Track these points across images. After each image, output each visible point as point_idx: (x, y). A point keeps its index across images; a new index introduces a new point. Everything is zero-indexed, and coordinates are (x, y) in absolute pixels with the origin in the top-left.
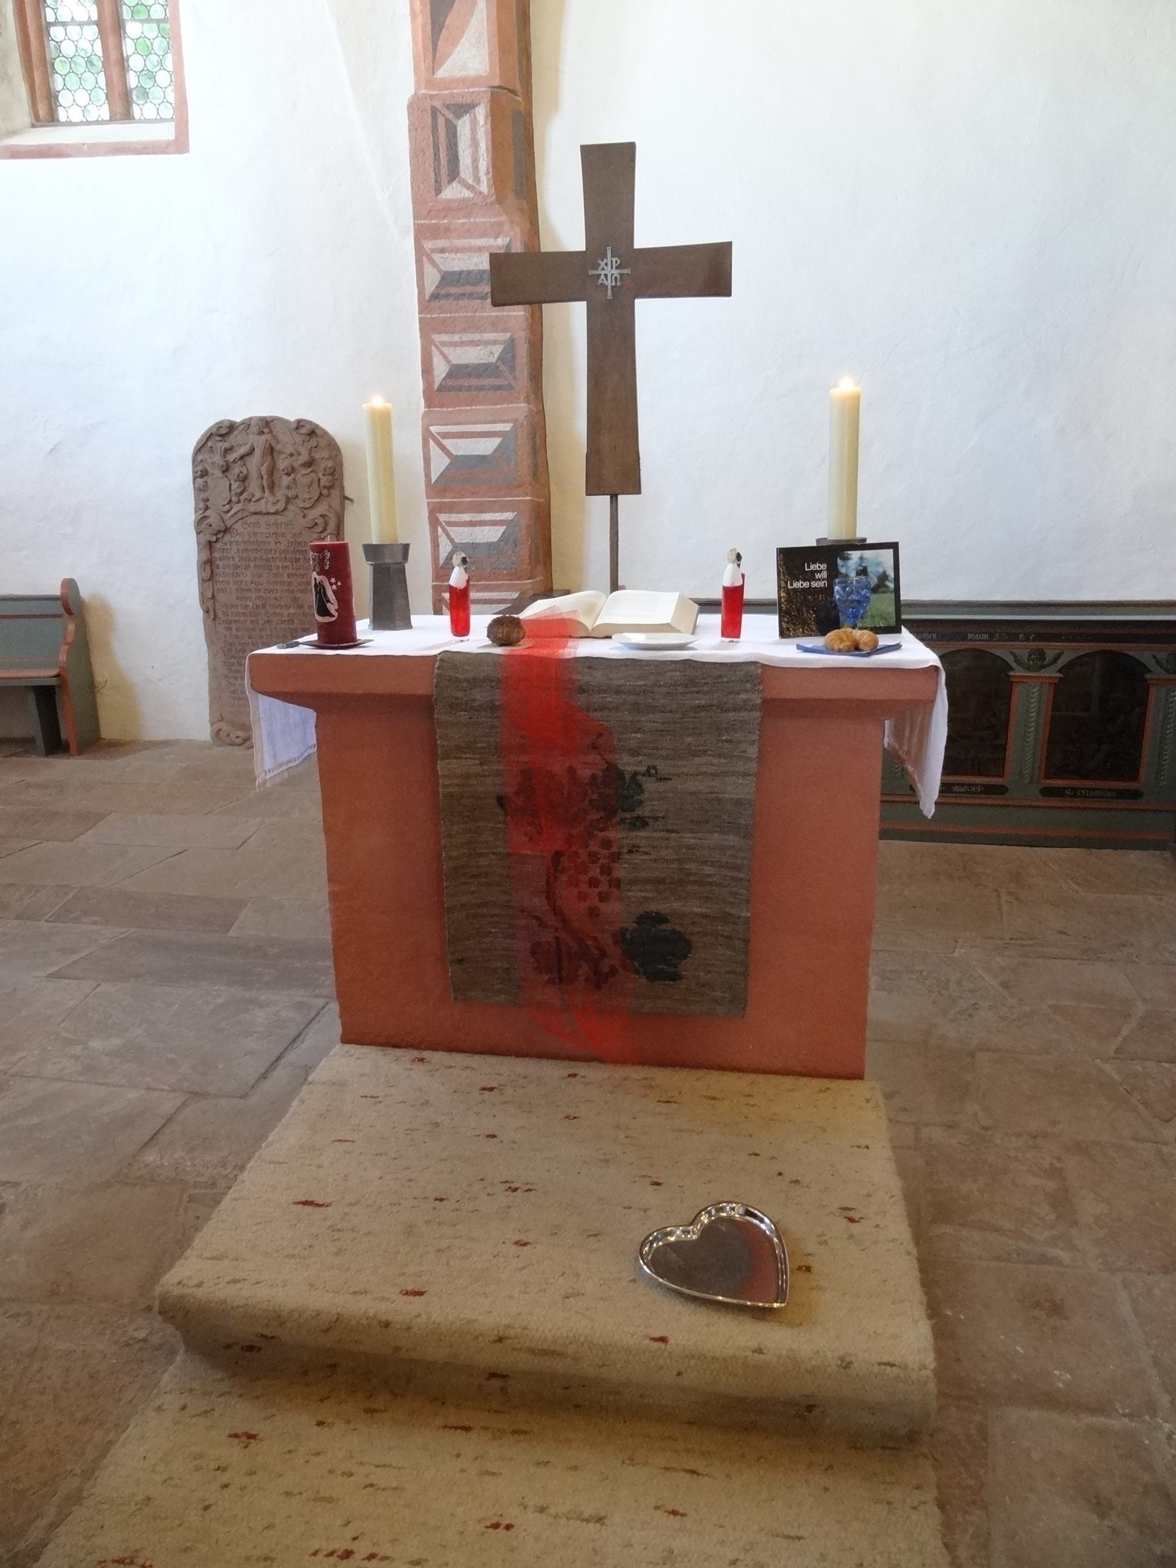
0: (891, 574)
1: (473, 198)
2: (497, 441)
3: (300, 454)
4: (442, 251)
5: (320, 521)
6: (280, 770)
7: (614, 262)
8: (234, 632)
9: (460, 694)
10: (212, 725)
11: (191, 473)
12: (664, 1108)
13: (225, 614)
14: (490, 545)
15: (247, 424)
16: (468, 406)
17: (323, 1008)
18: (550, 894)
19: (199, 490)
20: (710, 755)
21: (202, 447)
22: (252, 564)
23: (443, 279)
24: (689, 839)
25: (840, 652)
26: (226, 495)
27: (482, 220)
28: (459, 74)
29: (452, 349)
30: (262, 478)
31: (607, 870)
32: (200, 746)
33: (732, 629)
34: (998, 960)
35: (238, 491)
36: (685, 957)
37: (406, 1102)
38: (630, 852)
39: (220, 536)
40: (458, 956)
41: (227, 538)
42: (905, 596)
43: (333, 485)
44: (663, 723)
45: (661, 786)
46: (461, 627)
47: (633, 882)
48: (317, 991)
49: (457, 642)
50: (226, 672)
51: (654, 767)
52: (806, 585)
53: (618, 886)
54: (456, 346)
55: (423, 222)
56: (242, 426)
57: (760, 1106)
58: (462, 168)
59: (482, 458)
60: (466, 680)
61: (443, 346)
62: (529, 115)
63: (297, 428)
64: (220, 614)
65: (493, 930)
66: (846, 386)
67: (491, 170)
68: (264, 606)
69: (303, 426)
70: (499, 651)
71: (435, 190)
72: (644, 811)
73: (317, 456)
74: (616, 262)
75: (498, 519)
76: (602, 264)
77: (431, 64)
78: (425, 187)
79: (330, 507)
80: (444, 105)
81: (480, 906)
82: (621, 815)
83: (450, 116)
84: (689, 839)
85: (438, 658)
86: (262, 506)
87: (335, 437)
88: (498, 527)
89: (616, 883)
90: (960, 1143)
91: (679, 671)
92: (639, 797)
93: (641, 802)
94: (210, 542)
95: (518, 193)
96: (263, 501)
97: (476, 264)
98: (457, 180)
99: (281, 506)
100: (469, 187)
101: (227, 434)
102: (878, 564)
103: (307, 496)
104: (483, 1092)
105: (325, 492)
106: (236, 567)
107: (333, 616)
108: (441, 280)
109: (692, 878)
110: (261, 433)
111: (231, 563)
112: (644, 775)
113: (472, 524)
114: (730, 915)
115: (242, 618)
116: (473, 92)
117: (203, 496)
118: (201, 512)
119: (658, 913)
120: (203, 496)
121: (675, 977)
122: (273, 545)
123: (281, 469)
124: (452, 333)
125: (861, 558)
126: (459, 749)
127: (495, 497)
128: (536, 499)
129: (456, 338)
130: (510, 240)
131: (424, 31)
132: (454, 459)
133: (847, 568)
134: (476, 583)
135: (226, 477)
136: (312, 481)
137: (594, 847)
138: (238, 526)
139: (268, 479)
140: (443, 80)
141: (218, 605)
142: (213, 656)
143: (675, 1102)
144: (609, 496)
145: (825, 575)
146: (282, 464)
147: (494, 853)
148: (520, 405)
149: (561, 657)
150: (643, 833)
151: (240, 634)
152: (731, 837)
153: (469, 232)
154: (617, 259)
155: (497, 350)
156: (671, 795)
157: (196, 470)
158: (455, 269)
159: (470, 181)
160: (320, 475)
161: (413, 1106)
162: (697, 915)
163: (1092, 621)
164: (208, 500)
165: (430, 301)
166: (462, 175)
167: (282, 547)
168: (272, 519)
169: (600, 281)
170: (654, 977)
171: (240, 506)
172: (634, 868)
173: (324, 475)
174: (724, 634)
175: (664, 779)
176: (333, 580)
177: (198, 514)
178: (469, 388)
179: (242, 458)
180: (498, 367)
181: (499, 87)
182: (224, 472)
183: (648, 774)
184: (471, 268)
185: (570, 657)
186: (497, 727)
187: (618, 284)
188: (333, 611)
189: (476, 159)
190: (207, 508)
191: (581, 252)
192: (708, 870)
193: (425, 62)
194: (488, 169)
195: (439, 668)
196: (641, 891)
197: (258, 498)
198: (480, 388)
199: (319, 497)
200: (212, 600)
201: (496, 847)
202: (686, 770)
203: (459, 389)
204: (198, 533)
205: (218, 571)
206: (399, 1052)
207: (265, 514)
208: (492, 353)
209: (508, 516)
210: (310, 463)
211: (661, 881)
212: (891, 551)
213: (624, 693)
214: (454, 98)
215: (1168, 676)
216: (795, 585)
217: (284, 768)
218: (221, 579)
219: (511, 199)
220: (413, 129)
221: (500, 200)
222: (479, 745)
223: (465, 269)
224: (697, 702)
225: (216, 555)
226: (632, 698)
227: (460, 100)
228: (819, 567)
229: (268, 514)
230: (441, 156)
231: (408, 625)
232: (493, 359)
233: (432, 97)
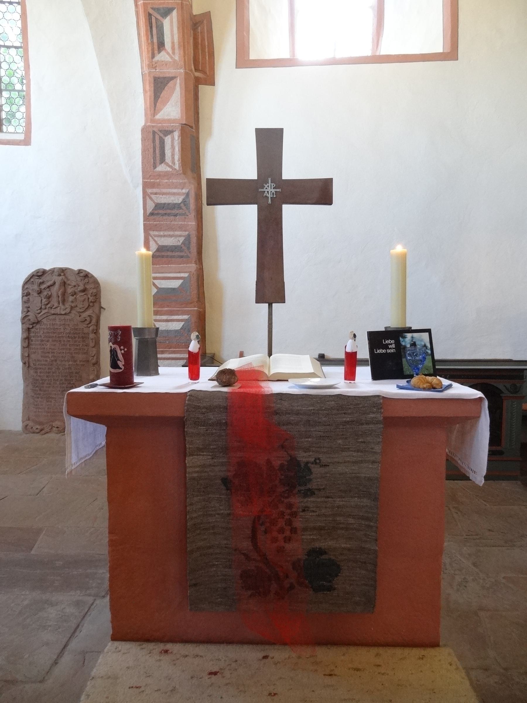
0: (428, 345)
1: (172, 171)
2: (181, 281)
3: (79, 286)
4: (156, 194)
5: (88, 319)
6: (81, 462)
7: (272, 186)
8: (39, 374)
9: (201, 416)
10: (23, 423)
11: (21, 294)
12: (328, 681)
13: (34, 364)
14: (176, 331)
15: (52, 271)
16: (166, 265)
17: (92, 604)
18: (254, 538)
19: (24, 302)
20: (352, 451)
21: (28, 281)
22: (51, 339)
23: (156, 206)
24: (339, 502)
25: (424, 389)
26: (39, 305)
27: (175, 181)
28: (166, 118)
29: (159, 238)
30: (59, 297)
31: (289, 523)
32: (16, 434)
33: (350, 375)
34: (283, 477)
35: (46, 303)
36: (337, 576)
37: (160, 690)
38: (304, 511)
39: (34, 325)
40: (193, 582)
41: (38, 326)
42: (437, 357)
43: (96, 301)
44: (324, 432)
45: (323, 470)
46: (194, 375)
47: (305, 529)
48: (88, 592)
49: (193, 383)
50: (33, 394)
51: (319, 459)
52: (384, 351)
53: (296, 532)
54: (161, 237)
55: (147, 180)
56: (50, 272)
57: (388, 674)
58: (167, 158)
59: (174, 289)
60: (204, 407)
61: (155, 237)
62: (198, 138)
63: (78, 273)
64: (32, 365)
65: (216, 563)
66: (399, 249)
67: (180, 159)
68: (56, 361)
69: (82, 272)
70: (225, 389)
71: (153, 167)
72: (313, 485)
73: (87, 287)
74: (273, 185)
75: (180, 318)
76: (266, 186)
77: (153, 113)
78: (149, 165)
79: (93, 311)
80: (159, 130)
81: (210, 547)
82: (299, 488)
83: (162, 135)
84: (339, 502)
85: (188, 395)
86: (58, 311)
87: (97, 279)
88: (180, 323)
89: (294, 530)
90: (496, 682)
91: (333, 401)
92: (309, 477)
93: (310, 480)
94: (29, 328)
95: (192, 171)
96: (59, 308)
97: (172, 201)
98: (164, 163)
99: (68, 310)
100: (170, 166)
101: (41, 276)
102: (422, 340)
103: (81, 306)
104: (210, 676)
105: (91, 304)
106: (42, 341)
107: (122, 369)
108: (155, 207)
109: (341, 526)
110: (60, 275)
111: (40, 339)
112: (312, 463)
113: (167, 321)
114: (364, 548)
115: (44, 367)
116: (173, 126)
117: (26, 305)
118: (25, 313)
119: (320, 548)
120: (26, 305)
121: (330, 589)
122: (62, 330)
123: (69, 293)
124: (160, 231)
125: (412, 337)
126: (199, 449)
127: (179, 308)
128: (199, 309)
129: (162, 233)
130: (189, 191)
131: (150, 99)
132: (160, 290)
133: (405, 342)
134: (168, 350)
135: (40, 296)
136: (85, 299)
137: (282, 508)
138: (44, 321)
139: (61, 297)
140: (159, 120)
141: (30, 360)
142: (26, 386)
143: (335, 675)
144: (267, 304)
145: (393, 346)
146: (70, 290)
147: (218, 514)
148: (192, 265)
149: (263, 394)
150: (312, 499)
151: (42, 374)
152: (365, 500)
153: (169, 186)
154: (274, 184)
155: (182, 239)
156: (328, 475)
157: (23, 292)
158: (162, 202)
159: (170, 164)
160: (90, 297)
161: (166, 693)
162: (344, 549)
163: (511, 369)
164: (29, 307)
165: (149, 216)
166: (167, 161)
167: (68, 331)
168: (62, 317)
169: (265, 195)
170: (316, 590)
171: (46, 311)
172: (306, 521)
173: (91, 296)
174: (346, 379)
175: (325, 466)
176: (122, 347)
177: (23, 314)
178: (167, 257)
179: (49, 287)
180: (182, 247)
181: (185, 124)
182: (38, 294)
183: (315, 463)
184: (170, 202)
185: (269, 393)
186: (223, 436)
187: (274, 196)
188: (121, 366)
189: (173, 154)
190: (28, 311)
191: (256, 180)
192: (351, 520)
193: (150, 111)
194: (179, 159)
195: (188, 400)
196: (310, 535)
197: (56, 306)
198: (172, 257)
199: (88, 307)
200: (28, 358)
201: (220, 510)
202: (336, 460)
203: (163, 257)
204: (23, 324)
205: (32, 343)
206: (151, 646)
207: (59, 315)
208: (179, 241)
209: (186, 317)
210: (84, 290)
211: (321, 529)
212: (427, 334)
213: (301, 414)
214: (163, 127)
215: (511, 395)
216: (378, 351)
217: (83, 461)
218: (33, 347)
219: (189, 173)
220: (144, 140)
221: (184, 173)
222: (212, 447)
223: (167, 202)
224: (345, 419)
225: (32, 334)
226: (305, 418)
227: (167, 129)
228: (390, 342)
229: (61, 314)
230: (157, 152)
231: (157, 373)
232: (179, 244)
233: (153, 127)
